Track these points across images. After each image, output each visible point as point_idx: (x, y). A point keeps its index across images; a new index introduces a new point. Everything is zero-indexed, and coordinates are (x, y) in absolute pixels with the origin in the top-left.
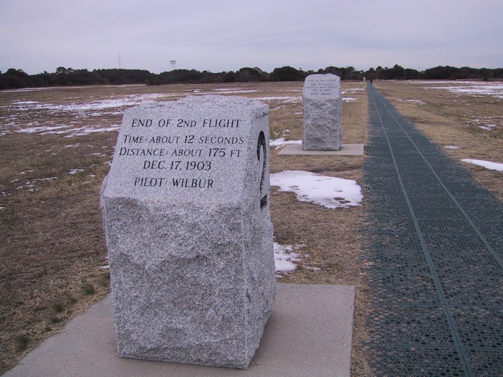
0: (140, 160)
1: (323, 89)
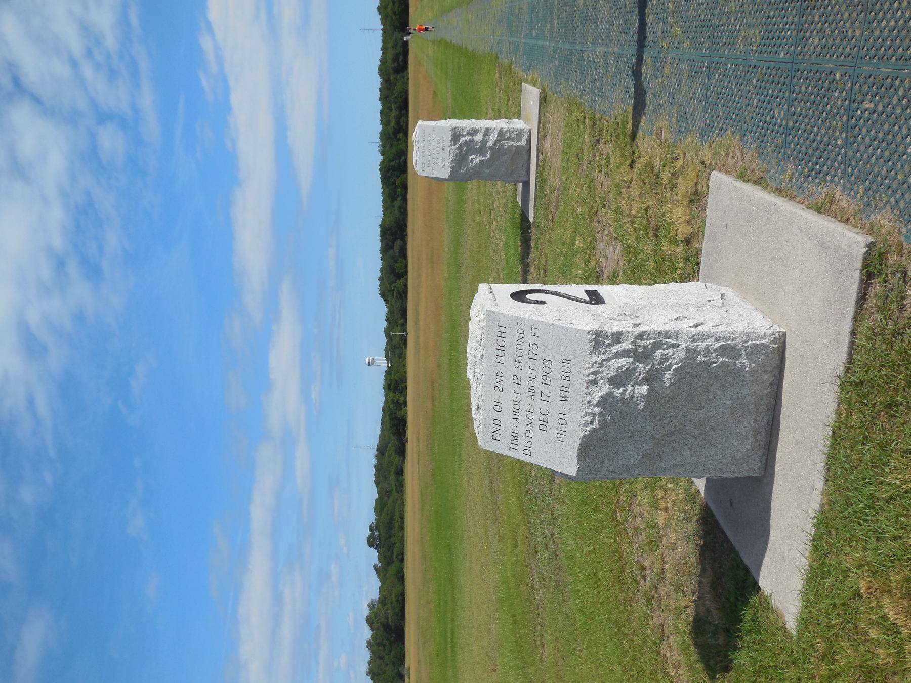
0: (537, 435)
1: (539, 387)
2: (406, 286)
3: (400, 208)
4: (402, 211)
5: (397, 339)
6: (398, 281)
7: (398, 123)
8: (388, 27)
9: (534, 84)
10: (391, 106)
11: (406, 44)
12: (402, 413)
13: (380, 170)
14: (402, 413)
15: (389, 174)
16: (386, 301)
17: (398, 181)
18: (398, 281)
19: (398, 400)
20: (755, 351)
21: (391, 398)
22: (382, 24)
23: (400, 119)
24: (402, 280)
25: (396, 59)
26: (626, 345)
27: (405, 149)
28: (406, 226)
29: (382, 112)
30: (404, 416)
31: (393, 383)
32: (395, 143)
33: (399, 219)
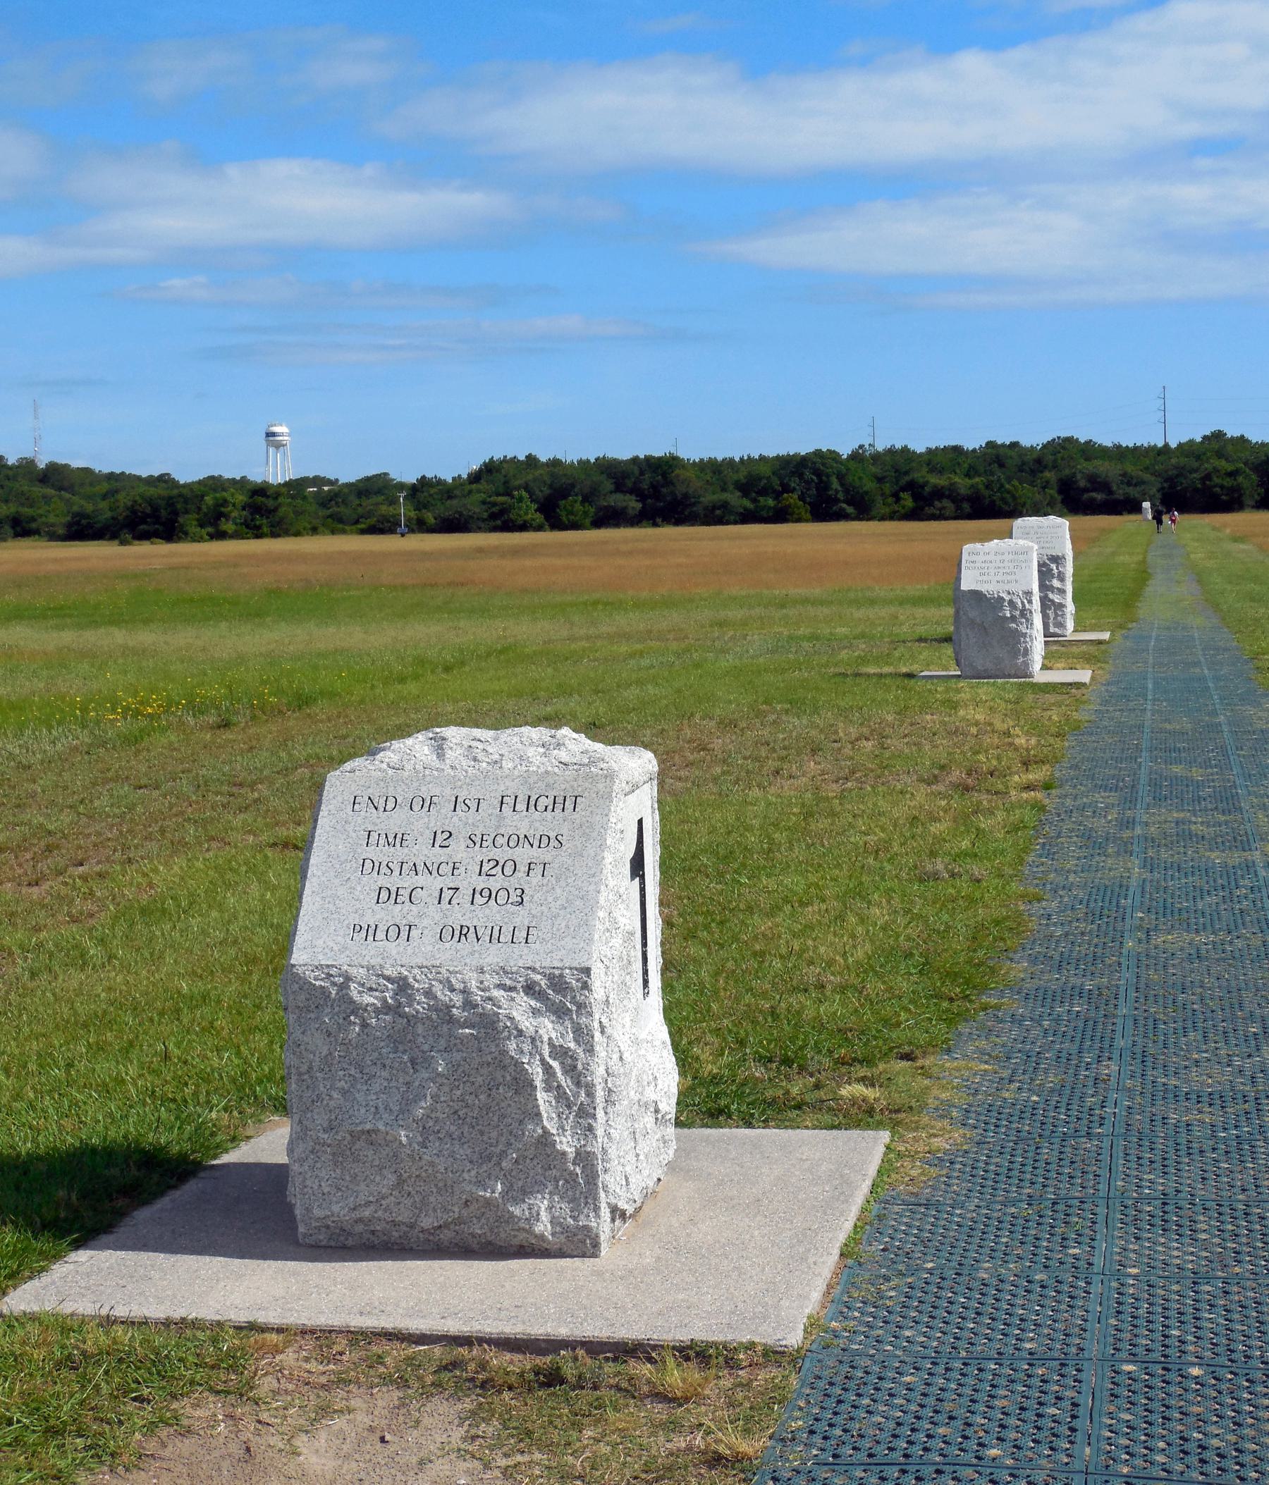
0: (977, 572)
1: (1001, 571)
2: (523, 527)
3: (725, 505)
4: (718, 512)
5: (384, 509)
6: (534, 506)
7: (938, 493)
8: (1174, 461)
9: (1093, 678)
10: (978, 474)
11: (1133, 507)
12: (194, 529)
13: (818, 453)
14: (194, 529)
15: (808, 475)
16: (475, 477)
17: (792, 499)
18: (534, 506)
19: (227, 516)
20: (1026, 664)
21: (230, 499)
22: (1180, 445)
23: (949, 497)
24: (539, 518)
25: (1098, 483)
26: (1027, 606)
27: (873, 513)
28: (678, 522)
29: (957, 450)
30: (186, 534)
31: (271, 503)
32: (887, 488)
33: (694, 504)
